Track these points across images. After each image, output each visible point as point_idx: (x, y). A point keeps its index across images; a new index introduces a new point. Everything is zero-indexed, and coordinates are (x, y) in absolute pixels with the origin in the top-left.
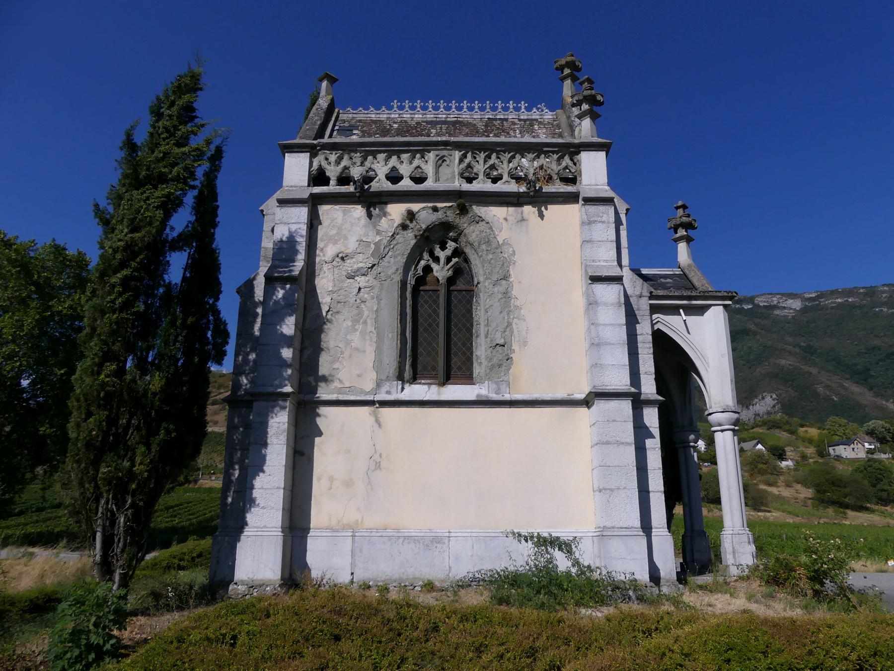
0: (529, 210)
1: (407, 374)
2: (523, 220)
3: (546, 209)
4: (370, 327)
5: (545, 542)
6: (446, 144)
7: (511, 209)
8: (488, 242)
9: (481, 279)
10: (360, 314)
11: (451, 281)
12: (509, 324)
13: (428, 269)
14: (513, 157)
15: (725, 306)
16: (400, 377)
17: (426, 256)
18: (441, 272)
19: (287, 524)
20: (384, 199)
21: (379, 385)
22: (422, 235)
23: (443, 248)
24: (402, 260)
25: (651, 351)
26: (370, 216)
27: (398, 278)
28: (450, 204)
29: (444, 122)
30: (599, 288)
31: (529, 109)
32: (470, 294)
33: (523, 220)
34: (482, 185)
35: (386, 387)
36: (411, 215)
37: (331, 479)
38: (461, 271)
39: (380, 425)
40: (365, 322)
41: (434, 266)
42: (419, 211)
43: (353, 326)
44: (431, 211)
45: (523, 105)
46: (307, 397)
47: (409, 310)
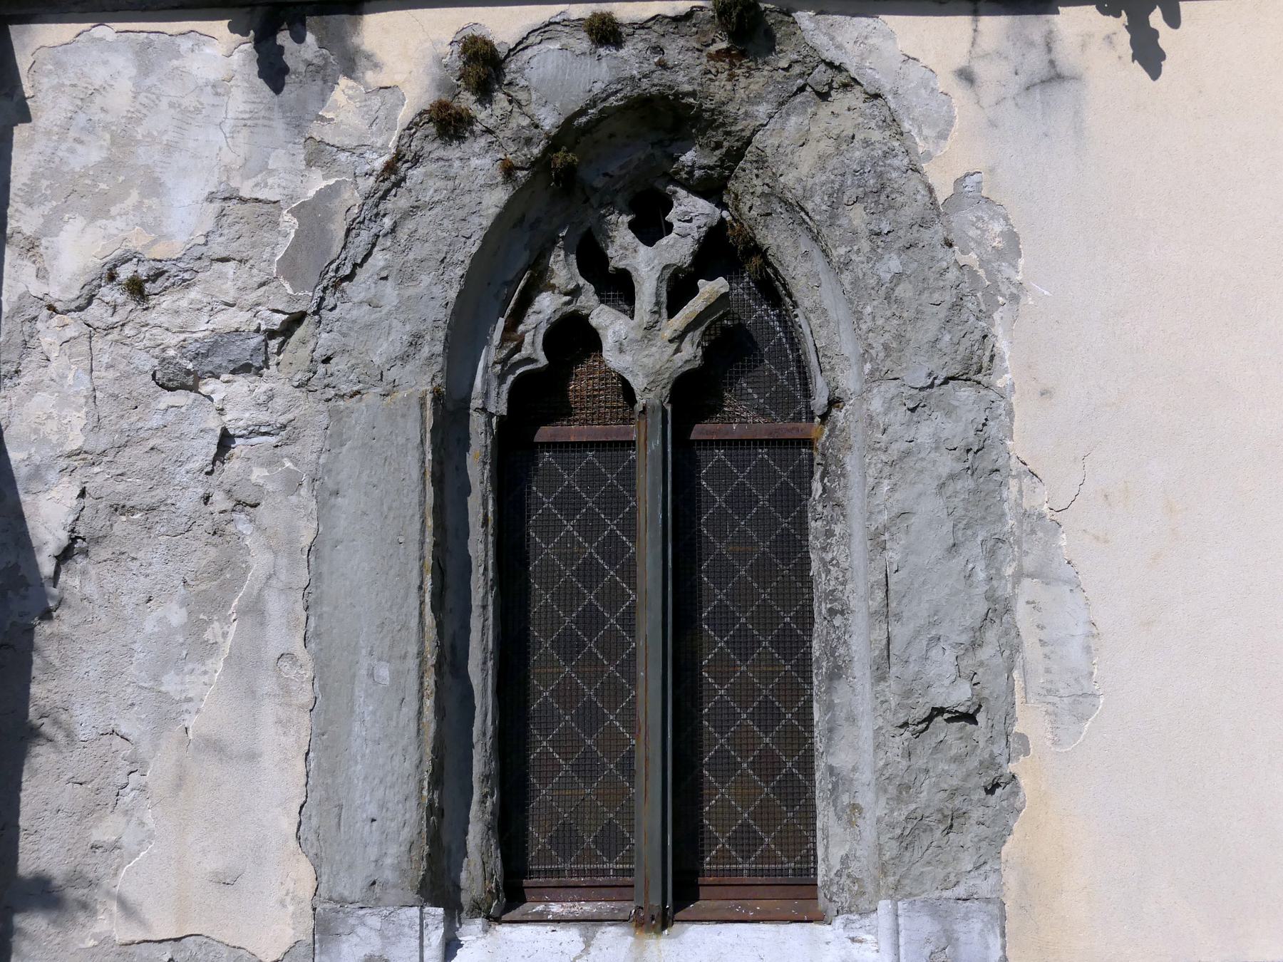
1: (477, 867)
2: (1055, 77)
4: (281, 633)
8: (879, 194)
9: (849, 381)
10: (227, 570)
11: (693, 395)
12: (998, 609)
13: (573, 338)
16: (438, 887)
17: (563, 269)
18: (641, 348)
22: (540, 166)
23: (651, 227)
24: (437, 293)
26: (273, 72)
27: (420, 380)
32: (794, 458)
33: (1055, 77)
36: (484, 66)
40: (255, 610)
41: (610, 324)
42: (521, 45)
43: (196, 627)
44: (582, 42)
47: (479, 547)
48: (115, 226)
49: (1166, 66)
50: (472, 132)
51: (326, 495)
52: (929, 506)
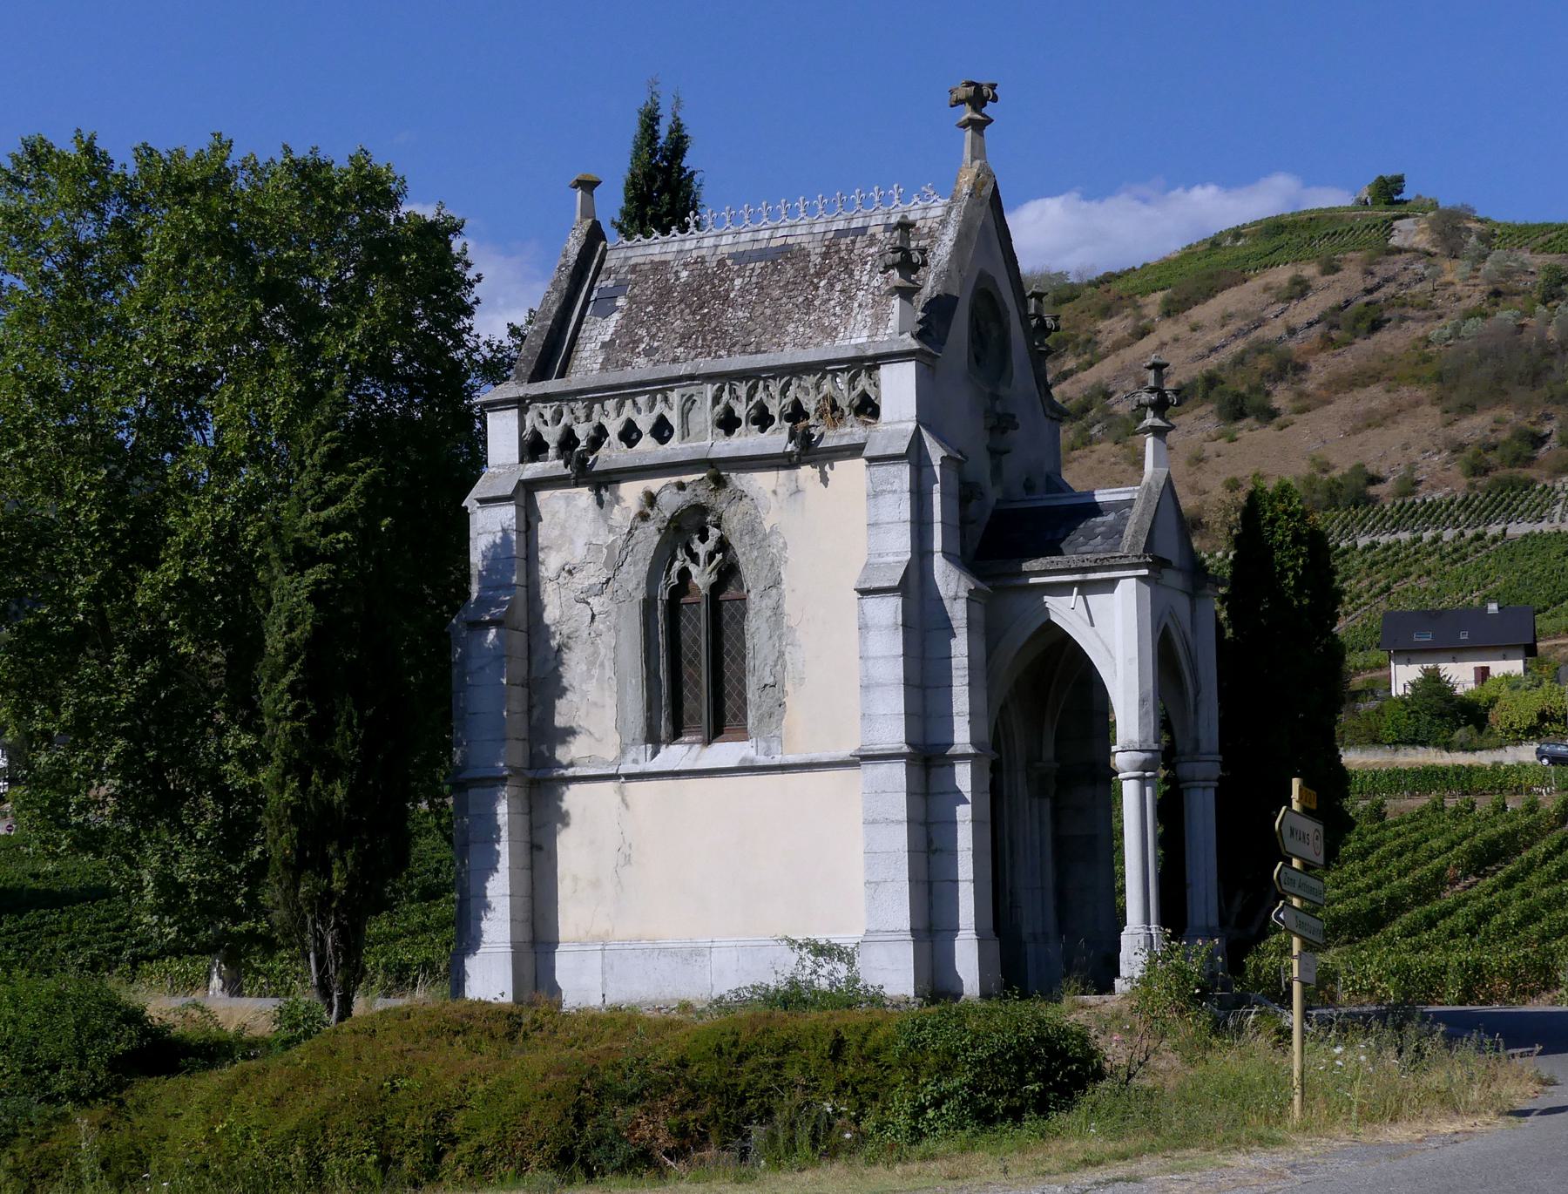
0: (807, 472)
1: (664, 729)
2: (798, 491)
3: (832, 468)
4: (609, 673)
5: (823, 951)
6: (691, 377)
7: (783, 473)
8: (753, 531)
10: (596, 653)
11: (716, 589)
12: (781, 654)
13: (685, 574)
14: (788, 384)
15: (1138, 577)
17: (681, 554)
18: (702, 578)
19: (525, 936)
20: (615, 478)
21: (623, 752)
22: (667, 528)
23: (704, 539)
24: (643, 568)
25: (966, 680)
26: (600, 503)
27: (640, 595)
28: (700, 476)
29: (762, 255)
30: (871, 602)
31: (905, 199)
33: (798, 491)
34: (747, 441)
35: (631, 755)
36: (651, 499)
37: (575, 879)
38: (728, 573)
39: (627, 806)
40: (602, 665)
41: (693, 569)
43: (589, 670)
45: (895, 191)
46: (540, 774)
48: (563, 554)
49: (1389, 173)
50: (112, 795)
51: (617, 632)
52: (764, 627)
